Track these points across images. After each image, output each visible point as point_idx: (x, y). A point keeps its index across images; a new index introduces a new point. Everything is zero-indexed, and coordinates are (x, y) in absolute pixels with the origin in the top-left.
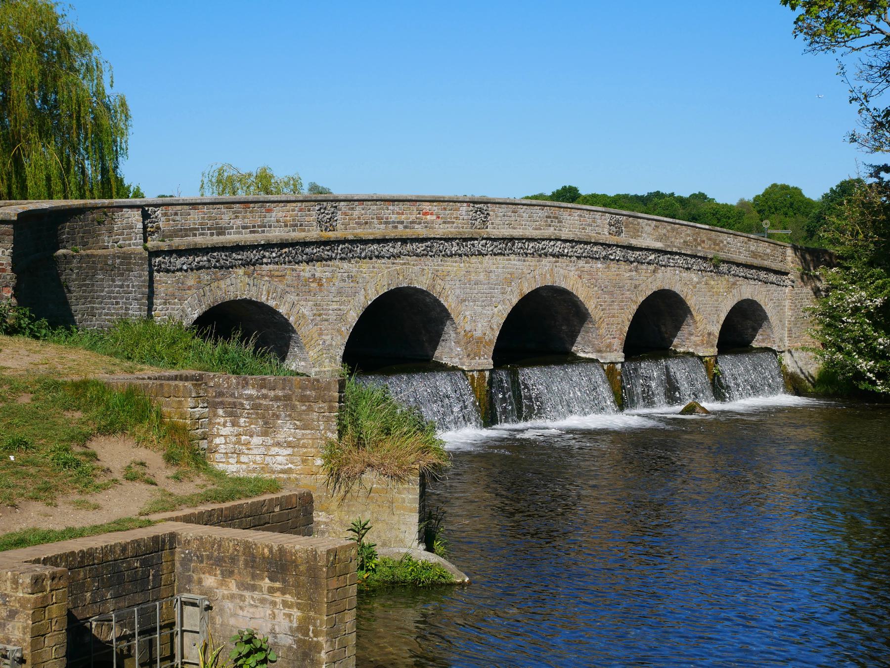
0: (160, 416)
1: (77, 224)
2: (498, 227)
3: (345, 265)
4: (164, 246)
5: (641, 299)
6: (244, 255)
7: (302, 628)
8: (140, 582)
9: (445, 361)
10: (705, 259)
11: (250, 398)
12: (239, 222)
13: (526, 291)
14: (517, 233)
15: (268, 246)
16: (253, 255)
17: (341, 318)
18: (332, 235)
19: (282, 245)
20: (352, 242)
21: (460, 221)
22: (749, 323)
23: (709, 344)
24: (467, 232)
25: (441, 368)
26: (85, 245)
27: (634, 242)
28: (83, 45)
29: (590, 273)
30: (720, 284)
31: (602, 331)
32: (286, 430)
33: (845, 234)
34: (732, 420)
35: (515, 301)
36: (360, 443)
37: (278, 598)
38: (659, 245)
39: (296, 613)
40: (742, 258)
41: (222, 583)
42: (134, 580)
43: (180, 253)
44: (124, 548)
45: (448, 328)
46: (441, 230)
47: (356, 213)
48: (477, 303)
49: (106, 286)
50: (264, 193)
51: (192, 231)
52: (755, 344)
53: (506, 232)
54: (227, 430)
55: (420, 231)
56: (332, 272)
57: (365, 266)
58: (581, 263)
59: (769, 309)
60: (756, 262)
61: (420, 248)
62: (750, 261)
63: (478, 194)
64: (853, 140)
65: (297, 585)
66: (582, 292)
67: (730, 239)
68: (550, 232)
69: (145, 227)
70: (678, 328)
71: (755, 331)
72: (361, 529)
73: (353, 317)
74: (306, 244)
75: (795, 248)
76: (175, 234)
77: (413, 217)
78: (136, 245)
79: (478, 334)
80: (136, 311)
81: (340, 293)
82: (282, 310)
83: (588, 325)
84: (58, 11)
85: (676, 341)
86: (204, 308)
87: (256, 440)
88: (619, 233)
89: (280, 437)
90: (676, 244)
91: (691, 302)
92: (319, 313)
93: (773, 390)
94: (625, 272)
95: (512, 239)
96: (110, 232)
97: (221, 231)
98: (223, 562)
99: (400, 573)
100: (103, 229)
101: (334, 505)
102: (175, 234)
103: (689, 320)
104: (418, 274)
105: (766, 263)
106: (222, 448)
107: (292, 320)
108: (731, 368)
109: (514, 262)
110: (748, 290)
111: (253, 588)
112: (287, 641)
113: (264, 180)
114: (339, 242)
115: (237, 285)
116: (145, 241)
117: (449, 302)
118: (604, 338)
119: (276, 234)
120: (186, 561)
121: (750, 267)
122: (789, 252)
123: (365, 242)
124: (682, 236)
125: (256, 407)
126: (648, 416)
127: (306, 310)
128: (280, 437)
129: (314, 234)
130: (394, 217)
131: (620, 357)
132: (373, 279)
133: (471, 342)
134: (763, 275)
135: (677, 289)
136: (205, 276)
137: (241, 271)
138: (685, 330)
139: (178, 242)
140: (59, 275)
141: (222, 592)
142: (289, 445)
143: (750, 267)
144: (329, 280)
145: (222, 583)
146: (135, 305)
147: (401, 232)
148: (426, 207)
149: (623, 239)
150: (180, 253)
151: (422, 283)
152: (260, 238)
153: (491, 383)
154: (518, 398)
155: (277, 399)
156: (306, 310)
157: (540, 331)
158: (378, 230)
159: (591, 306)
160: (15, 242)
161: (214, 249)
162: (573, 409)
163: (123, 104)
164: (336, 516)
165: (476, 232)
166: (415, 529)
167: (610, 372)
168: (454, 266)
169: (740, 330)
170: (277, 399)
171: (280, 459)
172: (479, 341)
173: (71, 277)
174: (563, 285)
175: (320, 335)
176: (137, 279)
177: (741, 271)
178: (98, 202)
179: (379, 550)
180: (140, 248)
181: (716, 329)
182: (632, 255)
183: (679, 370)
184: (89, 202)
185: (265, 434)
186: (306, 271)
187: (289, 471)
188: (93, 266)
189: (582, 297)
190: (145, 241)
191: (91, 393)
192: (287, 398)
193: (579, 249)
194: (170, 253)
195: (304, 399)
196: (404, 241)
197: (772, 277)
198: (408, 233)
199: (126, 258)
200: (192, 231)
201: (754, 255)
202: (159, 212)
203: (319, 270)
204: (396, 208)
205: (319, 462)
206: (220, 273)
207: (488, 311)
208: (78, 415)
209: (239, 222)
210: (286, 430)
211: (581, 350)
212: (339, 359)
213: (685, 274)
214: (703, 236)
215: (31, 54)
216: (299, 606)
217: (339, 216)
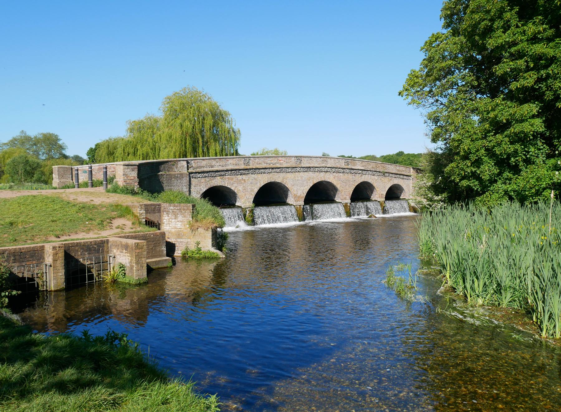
0: (133, 213)
1: (166, 165)
2: (305, 164)
3: (253, 175)
4: (194, 171)
5: (356, 184)
6: (220, 173)
7: (131, 262)
8: (98, 251)
9: (289, 202)
10: (380, 172)
11: (171, 209)
12: (218, 164)
13: (315, 182)
14: (311, 166)
15: (227, 171)
16: (223, 173)
17: (252, 190)
18: (248, 167)
19: (232, 170)
20: (255, 169)
21: (292, 162)
22: (399, 191)
23: (382, 197)
24: (294, 165)
25: (288, 204)
26: (168, 171)
27: (353, 167)
28: (227, 114)
29: (337, 177)
30: (386, 180)
31: (343, 194)
32: (180, 218)
33: (424, 164)
34: (390, 219)
35: (311, 185)
36: (197, 221)
37: (126, 254)
38: (363, 168)
39: (130, 258)
40: (394, 172)
41: (117, 251)
42: (95, 250)
43: (199, 173)
44: (91, 242)
45: (289, 193)
46: (285, 165)
47: (256, 161)
48: (298, 187)
49: (175, 182)
50: (277, 155)
51: (201, 167)
52: (401, 198)
53: (308, 165)
54: (166, 218)
55: (278, 166)
56: (251, 177)
57: (260, 176)
58: (335, 174)
59: (404, 187)
60: (399, 173)
61: (278, 170)
62: (396, 172)
63: (297, 155)
64: (427, 135)
65: (130, 251)
66: (335, 182)
67: (389, 166)
68: (323, 165)
69: (188, 166)
70: (372, 193)
71: (401, 193)
72: (198, 243)
73: (256, 190)
74: (240, 170)
75: (413, 168)
76: (198, 168)
77: (275, 162)
78: (185, 171)
79: (299, 195)
80: (185, 189)
81: (251, 183)
82: (232, 188)
83: (338, 192)
84: (218, 104)
85: (372, 197)
86: (207, 188)
87: (173, 220)
88: (348, 165)
89: (179, 220)
90: (369, 168)
91: (375, 185)
92: (245, 189)
93: (405, 211)
94: (350, 176)
95: (310, 167)
96: (177, 167)
97: (212, 167)
98: (117, 246)
99: (207, 255)
100: (174, 167)
101: (192, 237)
102: (198, 168)
103: (375, 190)
104: (277, 178)
105: (403, 173)
106: (165, 223)
107: (236, 191)
108: (389, 204)
109: (311, 174)
110: (396, 181)
111: (122, 252)
112: (128, 265)
113: (276, 152)
114: (251, 169)
115: (217, 182)
116: (188, 169)
117: (288, 185)
118: (344, 195)
119: (230, 167)
120: (111, 246)
121: (397, 174)
122: (412, 169)
123: (260, 169)
124: (371, 166)
125: (173, 212)
126: (358, 219)
127: (240, 188)
128: (179, 220)
129: (243, 167)
130: (269, 162)
131: (349, 201)
132: (263, 180)
133: (296, 197)
134: (401, 176)
135: (370, 181)
136: (207, 179)
137: (219, 178)
138: (374, 193)
139: (198, 170)
140: (159, 180)
141: (117, 253)
142: (181, 222)
143: (397, 174)
144: (248, 180)
145: (117, 251)
146: (185, 187)
147: (272, 166)
148: (280, 159)
149: (350, 167)
150: (199, 173)
151: (279, 180)
152: (225, 168)
153: (303, 209)
154: (312, 213)
155: (178, 209)
156: (240, 188)
157: (321, 194)
158: (264, 166)
159: (338, 186)
160: (138, 170)
161: (210, 172)
162: (330, 216)
163: (239, 131)
164: (192, 240)
165: (299, 165)
166: (211, 243)
167: (345, 206)
168: (289, 175)
169: (393, 194)
170: (178, 209)
171: (179, 225)
172: (299, 197)
173: (164, 180)
174: (328, 180)
175: (245, 195)
176: (186, 180)
177: (393, 175)
178: (173, 159)
179: (202, 249)
180: (186, 172)
181: (385, 193)
182: (352, 171)
183: (369, 204)
184: (171, 159)
185: (175, 219)
186: (240, 177)
187: (181, 228)
188: (170, 177)
189: (335, 184)
190: (188, 169)
191: (119, 207)
192: (180, 209)
193: (334, 170)
194: (196, 173)
195: (184, 209)
196: (273, 168)
197: (405, 177)
198: (274, 166)
199: (182, 175)
200: (201, 167)
201: (398, 170)
202: (192, 162)
203: (244, 177)
204: (270, 159)
205: (188, 226)
206: (212, 178)
207: (302, 188)
208: (115, 213)
209: (218, 164)
210: (180, 218)
211: (337, 199)
212: (252, 202)
213: (372, 177)
214: (379, 165)
215: (210, 117)
216: (130, 257)
217: (251, 162)
